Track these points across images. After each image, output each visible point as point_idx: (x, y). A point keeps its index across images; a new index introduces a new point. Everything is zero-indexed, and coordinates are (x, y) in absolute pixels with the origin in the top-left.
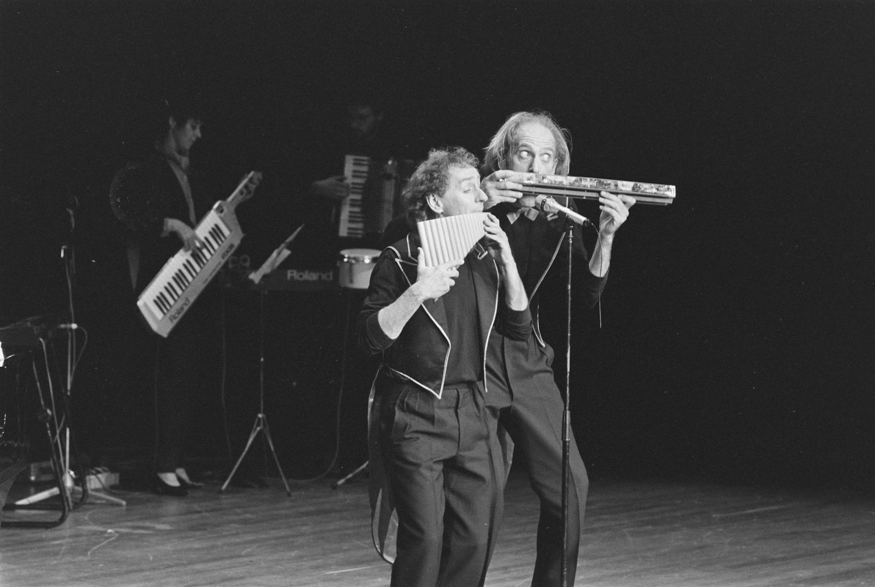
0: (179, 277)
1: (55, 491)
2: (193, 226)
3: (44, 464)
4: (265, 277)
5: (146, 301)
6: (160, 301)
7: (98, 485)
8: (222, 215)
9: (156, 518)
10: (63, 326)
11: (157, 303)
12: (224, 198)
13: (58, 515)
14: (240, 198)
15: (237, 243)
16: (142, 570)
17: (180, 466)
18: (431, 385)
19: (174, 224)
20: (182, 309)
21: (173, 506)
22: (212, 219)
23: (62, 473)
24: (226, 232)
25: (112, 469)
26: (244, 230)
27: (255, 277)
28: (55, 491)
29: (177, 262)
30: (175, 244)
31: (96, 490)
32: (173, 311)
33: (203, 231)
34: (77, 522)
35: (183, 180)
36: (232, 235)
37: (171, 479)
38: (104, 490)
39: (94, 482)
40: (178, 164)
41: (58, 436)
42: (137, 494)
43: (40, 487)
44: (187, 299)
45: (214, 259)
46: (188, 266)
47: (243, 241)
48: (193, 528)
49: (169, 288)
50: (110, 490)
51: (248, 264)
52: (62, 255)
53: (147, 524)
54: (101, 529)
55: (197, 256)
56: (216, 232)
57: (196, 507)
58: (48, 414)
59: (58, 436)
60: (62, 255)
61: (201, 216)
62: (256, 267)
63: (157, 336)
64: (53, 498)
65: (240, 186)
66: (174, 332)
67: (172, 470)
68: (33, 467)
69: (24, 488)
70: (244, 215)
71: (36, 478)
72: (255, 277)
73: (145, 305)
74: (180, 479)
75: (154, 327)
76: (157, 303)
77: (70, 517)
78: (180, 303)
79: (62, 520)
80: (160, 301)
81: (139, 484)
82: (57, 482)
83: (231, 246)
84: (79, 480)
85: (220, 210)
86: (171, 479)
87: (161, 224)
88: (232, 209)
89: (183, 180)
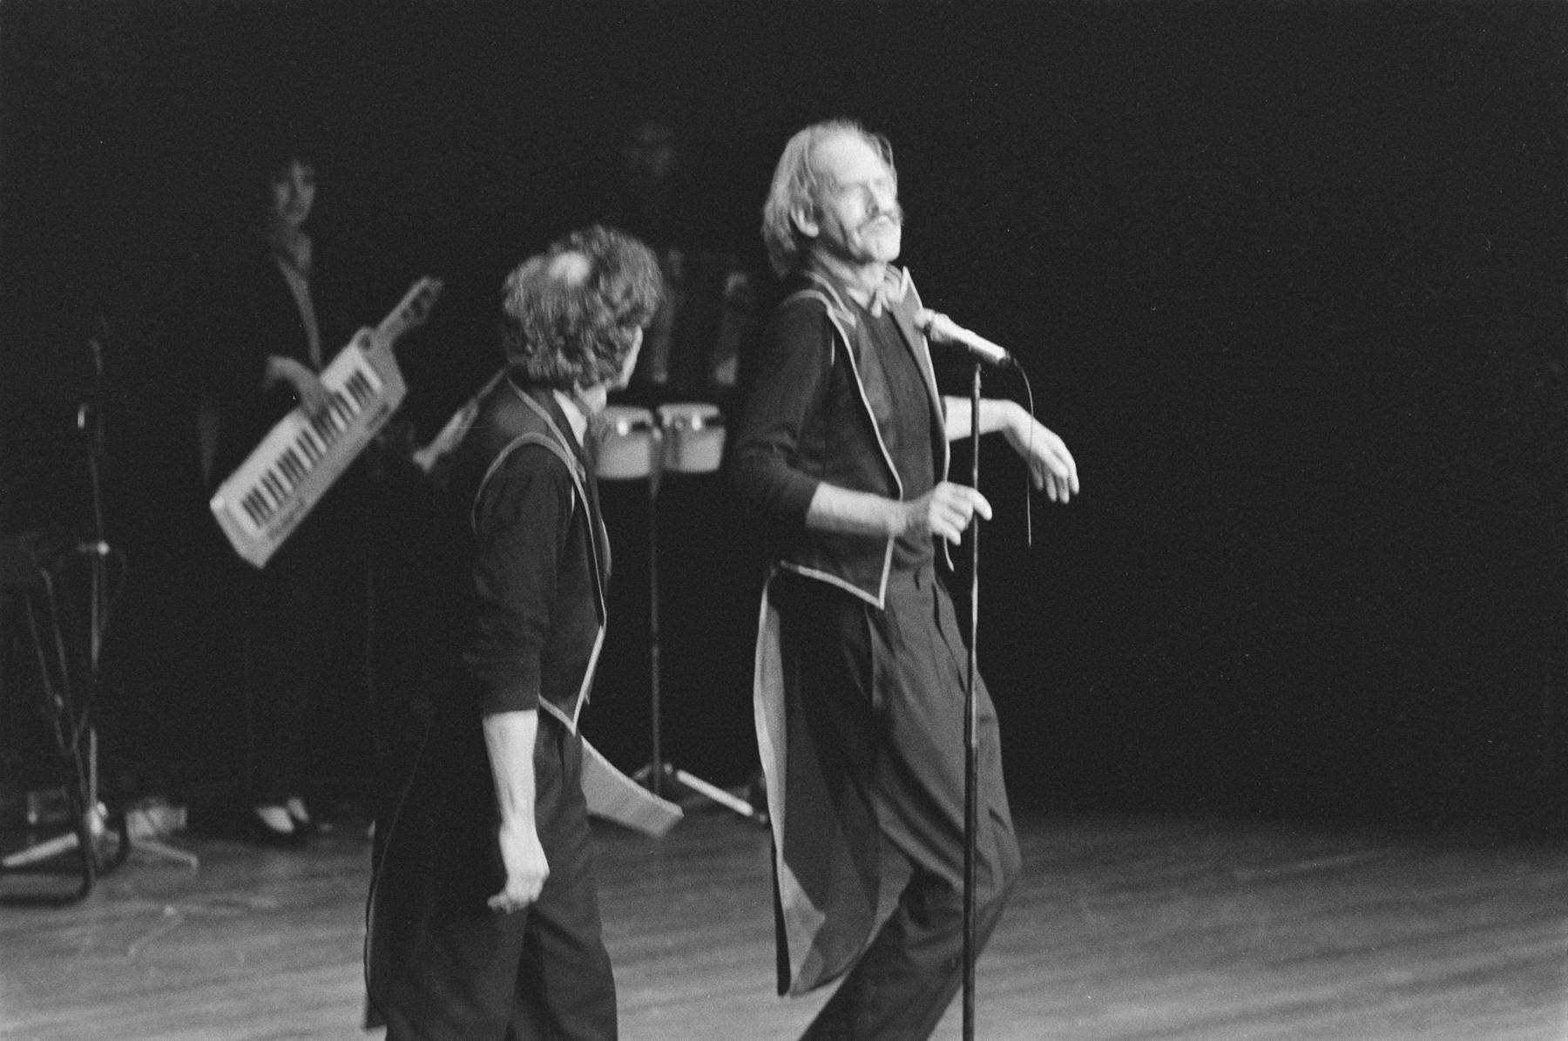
0: (289, 463)
1: (72, 840)
2: (317, 369)
3: (52, 794)
4: (442, 459)
5: (227, 502)
6: (254, 504)
7: (149, 830)
8: (371, 352)
9: (253, 885)
10: (83, 548)
11: (253, 505)
12: (374, 322)
13: (74, 885)
14: (402, 325)
15: (394, 402)
16: (225, 980)
17: (293, 793)
18: (847, 571)
19: (285, 366)
20: (291, 517)
21: (281, 866)
22: (351, 360)
23: (84, 807)
24: (375, 382)
25: (174, 801)
26: (408, 377)
27: (425, 459)
28: (72, 840)
29: (286, 434)
30: (285, 399)
31: (147, 838)
32: (276, 521)
33: (336, 377)
34: (112, 896)
35: (300, 288)
36: (388, 388)
37: (279, 819)
38: (161, 837)
39: (146, 823)
40: (291, 260)
41: (75, 745)
42: (218, 846)
43: (45, 833)
44: (301, 502)
45: (354, 430)
46: (305, 441)
47: (407, 401)
48: (316, 905)
49: (271, 481)
50: (173, 837)
51: (411, 436)
52: (951, 566)
53: (236, 896)
54: (149, 906)
55: (320, 421)
56: (358, 384)
57: (321, 866)
58: (55, 707)
59: (75, 745)
60: (951, 566)
61: (330, 352)
62: (426, 439)
63: (244, 566)
64: (70, 853)
65: (405, 303)
66: (276, 559)
67: (281, 802)
68: (32, 798)
69: (22, 835)
70: (406, 352)
71: (40, 817)
72: (425, 459)
73: (226, 510)
74: (293, 818)
75: (241, 548)
76: (253, 505)
77: (98, 888)
78: (290, 506)
79: (84, 892)
80: (254, 504)
81: (222, 826)
82: (77, 824)
83: (385, 408)
84: (116, 822)
85: (366, 344)
86: (279, 819)
87: (263, 366)
88: (388, 344)
89: (300, 288)
